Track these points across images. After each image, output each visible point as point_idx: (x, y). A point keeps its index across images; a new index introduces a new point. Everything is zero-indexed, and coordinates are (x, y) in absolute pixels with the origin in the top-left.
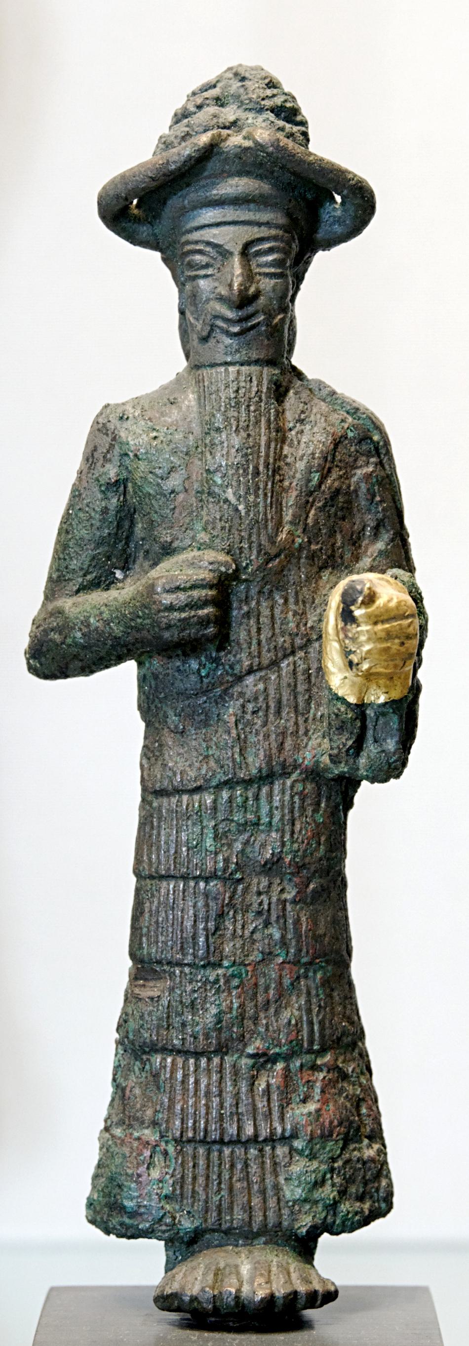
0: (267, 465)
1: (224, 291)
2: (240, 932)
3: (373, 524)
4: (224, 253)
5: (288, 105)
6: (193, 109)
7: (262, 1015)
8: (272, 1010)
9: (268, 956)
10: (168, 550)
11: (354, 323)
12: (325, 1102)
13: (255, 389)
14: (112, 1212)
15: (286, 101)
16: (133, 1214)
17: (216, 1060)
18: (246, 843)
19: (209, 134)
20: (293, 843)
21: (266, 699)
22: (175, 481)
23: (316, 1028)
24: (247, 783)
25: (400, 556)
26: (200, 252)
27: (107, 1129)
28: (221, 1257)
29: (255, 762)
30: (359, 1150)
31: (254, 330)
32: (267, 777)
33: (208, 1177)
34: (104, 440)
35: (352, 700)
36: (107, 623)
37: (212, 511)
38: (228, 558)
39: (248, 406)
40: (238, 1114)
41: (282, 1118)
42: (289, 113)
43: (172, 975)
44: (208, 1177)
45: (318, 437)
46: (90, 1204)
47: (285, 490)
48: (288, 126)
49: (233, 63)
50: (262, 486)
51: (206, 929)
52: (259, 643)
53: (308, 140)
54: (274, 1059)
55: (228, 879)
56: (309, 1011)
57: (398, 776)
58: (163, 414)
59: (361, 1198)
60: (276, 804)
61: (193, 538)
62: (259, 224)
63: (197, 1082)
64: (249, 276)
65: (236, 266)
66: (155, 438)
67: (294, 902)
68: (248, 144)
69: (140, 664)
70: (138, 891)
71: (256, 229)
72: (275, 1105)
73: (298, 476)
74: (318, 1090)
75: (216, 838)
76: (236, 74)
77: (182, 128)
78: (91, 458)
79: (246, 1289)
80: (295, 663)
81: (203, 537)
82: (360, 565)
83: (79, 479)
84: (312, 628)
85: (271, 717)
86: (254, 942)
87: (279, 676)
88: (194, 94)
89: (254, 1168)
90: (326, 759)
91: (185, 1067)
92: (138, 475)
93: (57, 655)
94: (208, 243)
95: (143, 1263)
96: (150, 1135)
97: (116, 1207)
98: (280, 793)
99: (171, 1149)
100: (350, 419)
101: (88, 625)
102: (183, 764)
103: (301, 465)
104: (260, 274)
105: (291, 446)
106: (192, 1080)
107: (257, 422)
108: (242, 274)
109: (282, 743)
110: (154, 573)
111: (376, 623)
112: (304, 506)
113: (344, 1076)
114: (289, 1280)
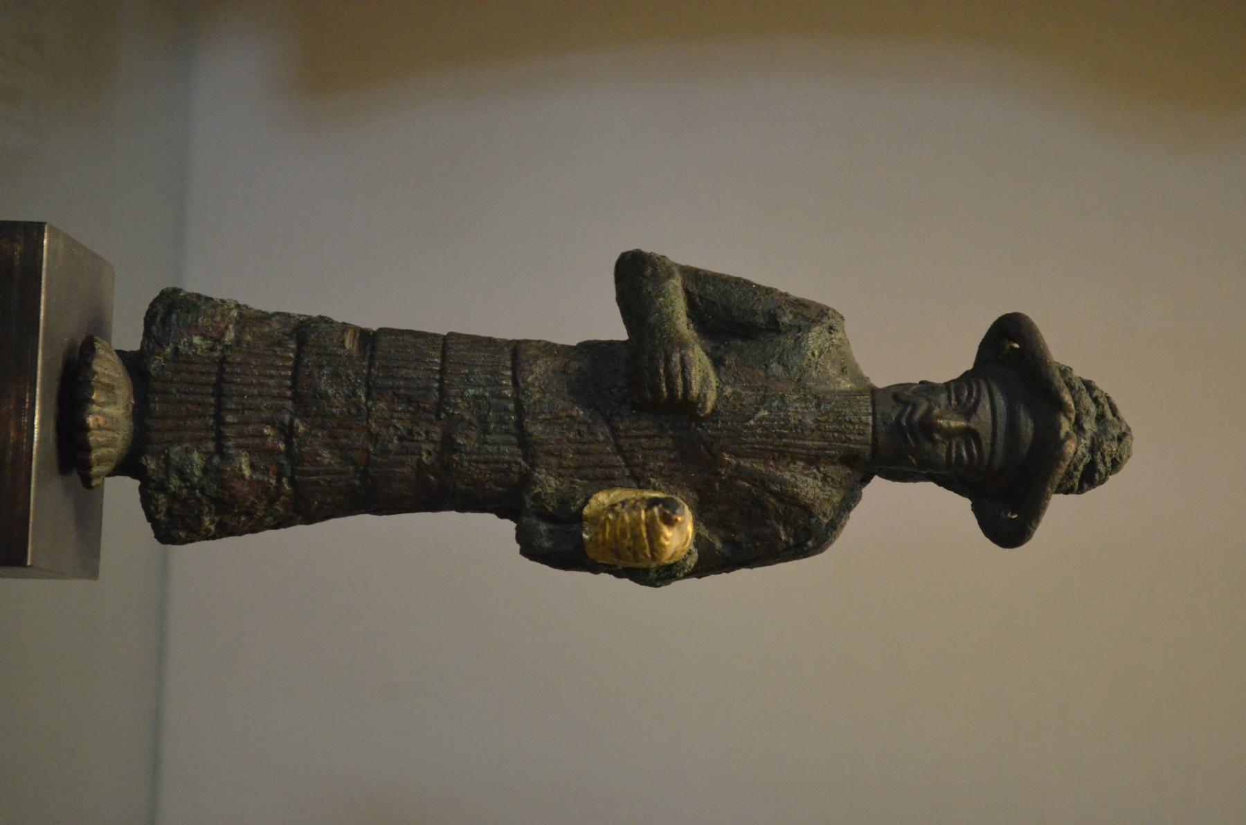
0: (785, 445)
1: (936, 411)
2: (395, 415)
3: (737, 538)
4: (969, 413)
5: (1097, 476)
6: (1095, 394)
7: (325, 432)
8: (329, 441)
9: (374, 438)
10: (717, 363)
11: (909, 523)
12: (251, 482)
13: (852, 437)
14: (170, 309)
15: (1100, 474)
16: (164, 322)
17: (289, 393)
18: (470, 423)
19: (1071, 403)
20: (469, 461)
21: (591, 442)
22: (776, 368)
23: (314, 478)
24: (519, 424)
25: (709, 563)
26: (970, 394)
27: (238, 306)
28: (124, 392)
29: (536, 430)
30: (210, 512)
31: (902, 438)
32: (524, 441)
33: (191, 383)
34: (812, 315)
35: (586, 511)
36: (659, 311)
37: (749, 397)
38: (708, 411)
39: (838, 431)
40: (243, 410)
41: (238, 446)
42: (1089, 478)
43: (363, 358)
44: (191, 383)
45: (811, 492)
46: (176, 291)
47: (766, 463)
48: (1078, 474)
49: (1134, 433)
50: (770, 440)
51: (399, 387)
52: (638, 437)
53: (1066, 493)
54: (288, 443)
55: (439, 408)
56: (327, 473)
57: (523, 552)
58: (833, 362)
59: (169, 513)
60: (502, 448)
61: (727, 383)
62: (993, 444)
63: (271, 377)
64: (949, 434)
65: (958, 423)
66: (813, 354)
67: (420, 461)
68: (1063, 434)
69: (624, 342)
70: (435, 335)
71: (989, 441)
72: (250, 441)
73: (778, 473)
74: (261, 477)
75: (475, 396)
76: (1124, 434)
77: (1078, 384)
78: (799, 304)
79: (95, 408)
80: (620, 467)
81: (728, 391)
82: (702, 527)
83: (781, 294)
84: (649, 482)
85: (574, 446)
86: (387, 428)
87: (608, 453)
88: (1108, 398)
89: (197, 422)
90: (537, 490)
91: (285, 368)
92: (782, 339)
93: (635, 276)
94: (977, 401)
95: (127, 333)
96: (230, 336)
97: (171, 308)
98: (509, 452)
99: (216, 354)
100: (826, 521)
101: (658, 297)
102: (538, 372)
103: (787, 475)
104: (950, 444)
105: (804, 468)
106: (273, 372)
107: (824, 439)
108: (950, 427)
109: (552, 455)
110: (698, 349)
111: (647, 525)
112: (753, 478)
113: (272, 501)
114: (101, 446)
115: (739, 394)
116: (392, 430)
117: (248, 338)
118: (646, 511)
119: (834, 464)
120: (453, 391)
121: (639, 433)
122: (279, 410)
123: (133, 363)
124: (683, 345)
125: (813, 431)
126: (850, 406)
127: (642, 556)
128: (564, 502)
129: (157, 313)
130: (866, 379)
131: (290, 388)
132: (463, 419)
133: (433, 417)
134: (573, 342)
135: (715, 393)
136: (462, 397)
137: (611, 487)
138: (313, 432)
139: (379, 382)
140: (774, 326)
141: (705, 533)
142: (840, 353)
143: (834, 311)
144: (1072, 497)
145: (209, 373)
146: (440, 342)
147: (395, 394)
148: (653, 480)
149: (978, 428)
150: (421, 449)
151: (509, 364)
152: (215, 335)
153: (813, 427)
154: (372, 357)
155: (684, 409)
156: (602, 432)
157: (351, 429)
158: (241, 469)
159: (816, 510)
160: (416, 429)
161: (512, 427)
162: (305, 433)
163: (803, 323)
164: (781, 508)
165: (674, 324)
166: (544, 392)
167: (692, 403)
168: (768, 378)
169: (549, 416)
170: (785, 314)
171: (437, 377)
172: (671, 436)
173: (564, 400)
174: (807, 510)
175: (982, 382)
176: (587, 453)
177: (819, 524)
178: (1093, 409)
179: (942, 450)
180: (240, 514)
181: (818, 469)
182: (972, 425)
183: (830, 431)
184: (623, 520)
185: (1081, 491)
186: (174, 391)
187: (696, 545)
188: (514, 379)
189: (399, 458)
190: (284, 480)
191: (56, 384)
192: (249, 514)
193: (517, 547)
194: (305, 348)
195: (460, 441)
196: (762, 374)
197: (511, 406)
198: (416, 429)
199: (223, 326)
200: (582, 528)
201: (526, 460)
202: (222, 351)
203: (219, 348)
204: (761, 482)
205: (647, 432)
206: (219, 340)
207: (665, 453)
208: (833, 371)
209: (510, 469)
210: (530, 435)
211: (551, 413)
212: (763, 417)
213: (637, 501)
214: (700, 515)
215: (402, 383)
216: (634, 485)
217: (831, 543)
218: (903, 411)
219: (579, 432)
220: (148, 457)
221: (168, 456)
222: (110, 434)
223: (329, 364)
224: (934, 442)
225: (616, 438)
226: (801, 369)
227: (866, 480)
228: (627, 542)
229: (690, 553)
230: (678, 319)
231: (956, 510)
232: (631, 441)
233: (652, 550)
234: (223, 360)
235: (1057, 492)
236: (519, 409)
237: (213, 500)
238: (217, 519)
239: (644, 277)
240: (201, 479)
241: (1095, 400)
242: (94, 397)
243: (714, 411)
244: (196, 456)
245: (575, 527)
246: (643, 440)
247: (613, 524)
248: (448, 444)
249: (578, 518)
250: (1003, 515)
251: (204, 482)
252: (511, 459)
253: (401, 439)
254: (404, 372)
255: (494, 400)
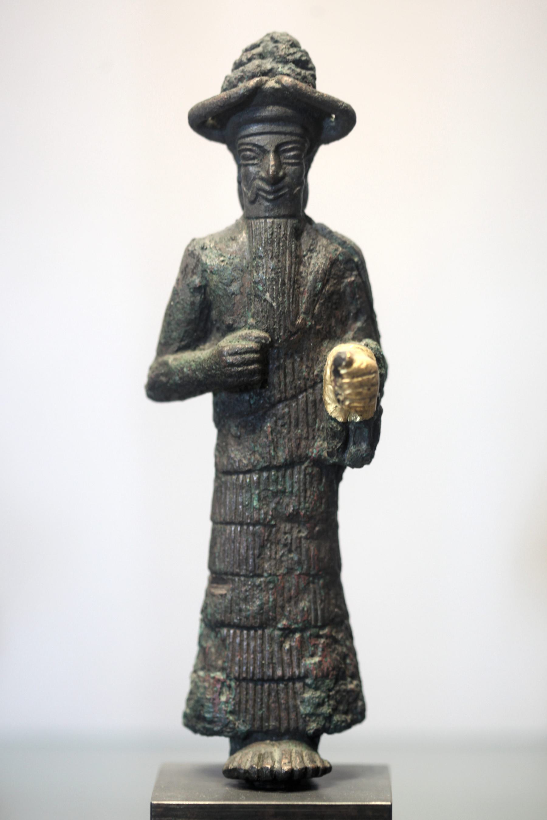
0: (290, 279)
1: (263, 174)
2: (273, 556)
3: (354, 311)
4: (263, 151)
5: (304, 58)
7: (287, 605)
9: (290, 571)
10: (231, 329)
11: (339, 188)
12: (324, 656)
13: (282, 233)
14: (198, 719)
15: (302, 56)
16: (211, 722)
18: (278, 503)
19: (256, 80)
20: (305, 503)
22: (234, 288)
23: (319, 613)
24: (278, 468)
25: (371, 331)
26: (250, 150)
27: (195, 671)
28: (263, 747)
29: (282, 456)
31: (278, 197)
32: (290, 464)
33: (255, 701)
34: (192, 262)
35: (340, 419)
36: (194, 371)
37: (255, 306)
38: (267, 335)
39: (279, 243)
40: (273, 663)
41: (299, 666)
42: (304, 63)
44: (255, 701)
46: (185, 716)
47: (302, 293)
48: (303, 72)
49: (270, 30)
51: (253, 554)
54: (294, 631)
55: (267, 525)
56: (315, 603)
59: (346, 713)
60: (295, 480)
61: (246, 322)
62: (285, 134)
63: (248, 645)
64: (279, 165)
65: (271, 160)
66: (223, 261)
67: (306, 538)
68: (277, 86)
69: (215, 395)
70: (214, 531)
71: (283, 137)
73: (309, 284)
74: (320, 649)
75: (259, 500)
76: (272, 38)
77: (238, 73)
79: (277, 766)
80: (307, 396)
81: (251, 321)
84: (317, 375)
85: (292, 428)
86: (282, 562)
87: (297, 404)
88: (247, 50)
89: (282, 695)
90: (325, 454)
91: (241, 635)
92: (212, 284)
93: (165, 388)
94: (254, 145)
96: (219, 675)
97: (200, 718)
99: (233, 684)
100: (340, 249)
103: (310, 278)
104: (286, 163)
105: (304, 266)
106: (245, 643)
107: (284, 253)
108: (275, 165)
109: (299, 444)
111: (353, 377)
112: (312, 302)
113: (336, 641)
114: (302, 761)
115: (254, 313)
116: (284, 558)
117: (220, 662)
118: (343, 378)
119: (300, 245)
120: (256, 516)
121: (282, 384)
122: (271, 638)
123: (240, 742)
124: (220, 354)
125: (279, 261)
126: (260, 234)
127: (374, 380)
128: (334, 435)
129: (204, 728)
130: (237, 224)
131: (256, 631)
132: (275, 509)
133: (274, 530)
134: (214, 432)
135: (253, 331)
136: (259, 509)
137: (322, 401)
138: (287, 614)
139: (250, 568)
140: (202, 289)
141: (350, 334)
142: (221, 242)
143: (190, 245)
144: (318, 74)
145: (247, 689)
146: (219, 526)
147: (259, 557)
148: (316, 373)
149: (276, 143)
150: (297, 537)
151: (234, 477)
152: (219, 686)
153: (275, 260)
154: (233, 574)
155: (265, 351)
156: (282, 409)
157: (283, 587)
158: (315, 664)
159: (334, 257)
160: (283, 541)
161: (280, 474)
162: (288, 619)
163: (200, 268)
164: (332, 282)
165: (204, 360)
166: (254, 452)
167: (261, 347)
168: (241, 293)
169: (272, 448)
170: (193, 282)
171: (245, 527)
172: (285, 361)
173: (260, 437)
174: (333, 263)
175: (240, 142)
176: (297, 420)
177: (343, 253)
178: (257, 62)
179: (290, 169)
180: (345, 663)
181: (304, 256)
182: (272, 149)
183: (279, 249)
184: (349, 394)
185: (313, 69)
186: (260, 713)
187: (360, 340)
188: (245, 473)
189: (304, 552)
190: (321, 633)
191: (260, 793)
192: (344, 657)
193: (366, 467)
194: (227, 622)
195: (291, 509)
196: (238, 297)
197: (265, 474)
198: (283, 541)
199: (212, 681)
200: (352, 422)
201: (303, 463)
202: (231, 680)
203: (228, 682)
204: (315, 296)
205: (282, 377)
206: (223, 683)
207: (296, 365)
208: (234, 247)
209: (310, 474)
210: (286, 460)
211: (269, 446)
212: (271, 296)
213: (336, 385)
214: (338, 338)
215: (251, 552)
216: (320, 385)
217: (354, 244)
218: (263, 197)
219: (283, 426)
220: (308, 728)
221: (307, 715)
222: (294, 755)
223: (238, 604)
224: (285, 175)
225: (286, 399)
226: (234, 270)
227: (309, 220)
228: (365, 391)
229: (367, 345)
230: (199, 358)
231: (327, 157)
232: (289, 388)
233: (370, 373)
234: (237, 679)
235: (314, 87)
236: (267, 468)
237: (336, 683)
238: (349, 679)
239: (168, 382)
240: (322, 692)
241: (250, 60)
242: (269, 767)
243: (267, 331)
244: (307, 695)
245: (352, 427)
246: (288, 380)
247: (352, 401)
248: (293, 518)
249: (345, 425)
250: (334, 124)
251: (324, 688)
252: (302, 473)
253: (290, 551)
254: (243, 551)
255: (262, 487)
